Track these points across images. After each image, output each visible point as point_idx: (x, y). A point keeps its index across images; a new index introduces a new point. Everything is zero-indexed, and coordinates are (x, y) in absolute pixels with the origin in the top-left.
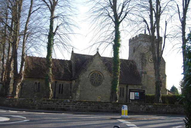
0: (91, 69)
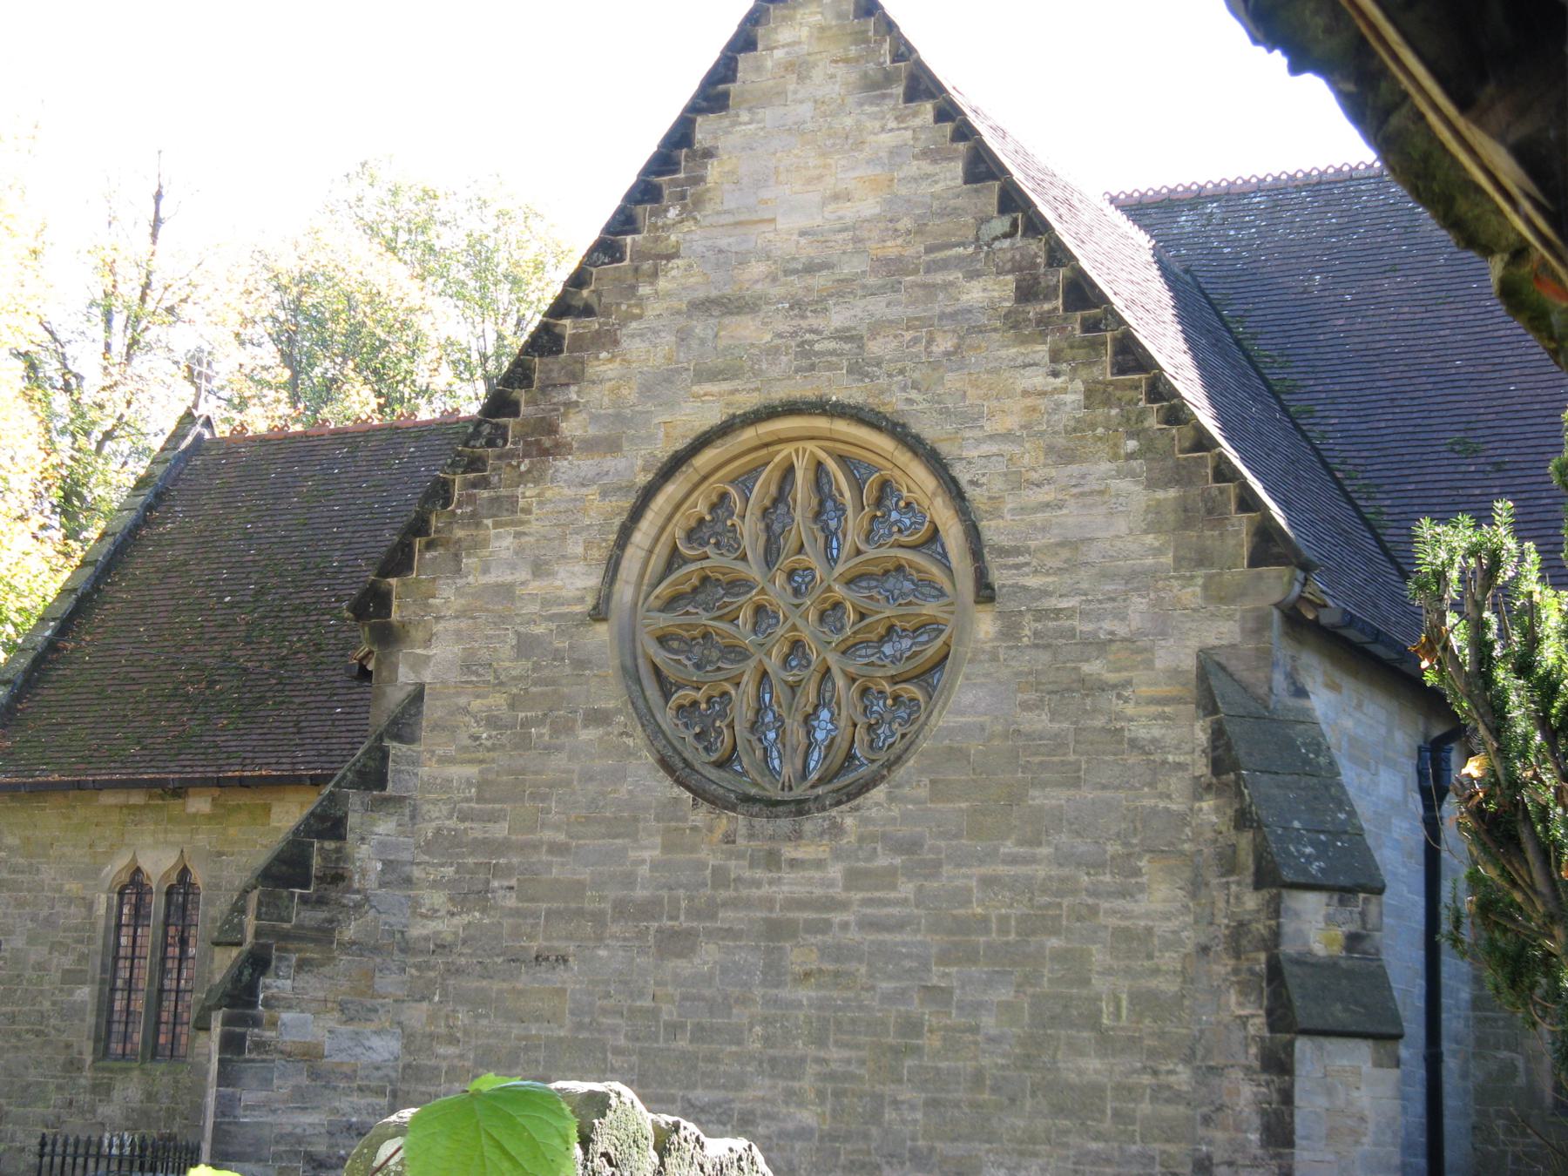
0: (659, 385)
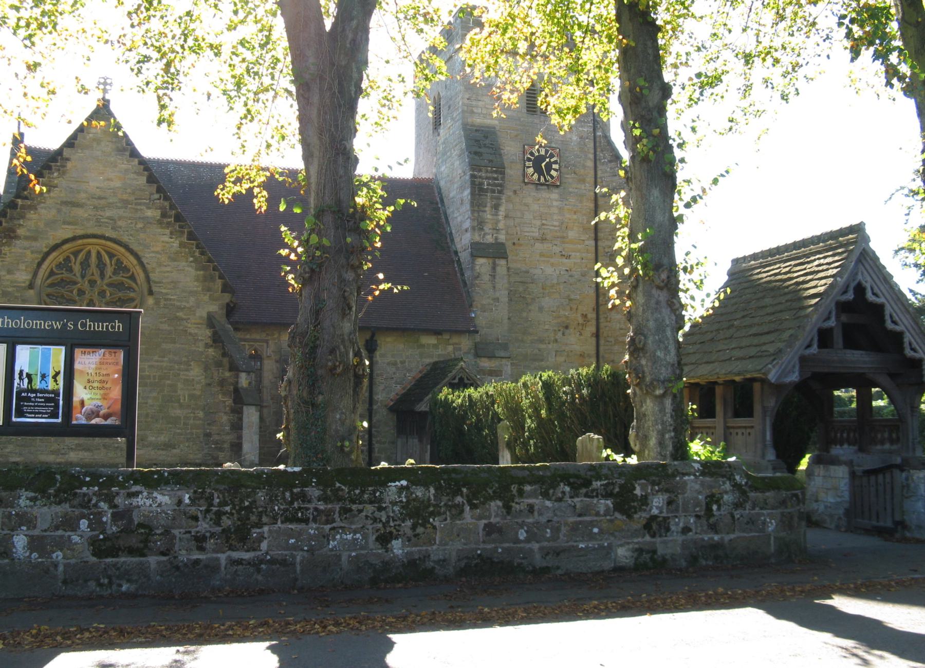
0: (51, 224)
